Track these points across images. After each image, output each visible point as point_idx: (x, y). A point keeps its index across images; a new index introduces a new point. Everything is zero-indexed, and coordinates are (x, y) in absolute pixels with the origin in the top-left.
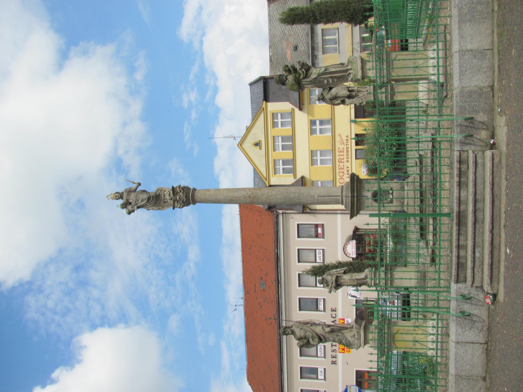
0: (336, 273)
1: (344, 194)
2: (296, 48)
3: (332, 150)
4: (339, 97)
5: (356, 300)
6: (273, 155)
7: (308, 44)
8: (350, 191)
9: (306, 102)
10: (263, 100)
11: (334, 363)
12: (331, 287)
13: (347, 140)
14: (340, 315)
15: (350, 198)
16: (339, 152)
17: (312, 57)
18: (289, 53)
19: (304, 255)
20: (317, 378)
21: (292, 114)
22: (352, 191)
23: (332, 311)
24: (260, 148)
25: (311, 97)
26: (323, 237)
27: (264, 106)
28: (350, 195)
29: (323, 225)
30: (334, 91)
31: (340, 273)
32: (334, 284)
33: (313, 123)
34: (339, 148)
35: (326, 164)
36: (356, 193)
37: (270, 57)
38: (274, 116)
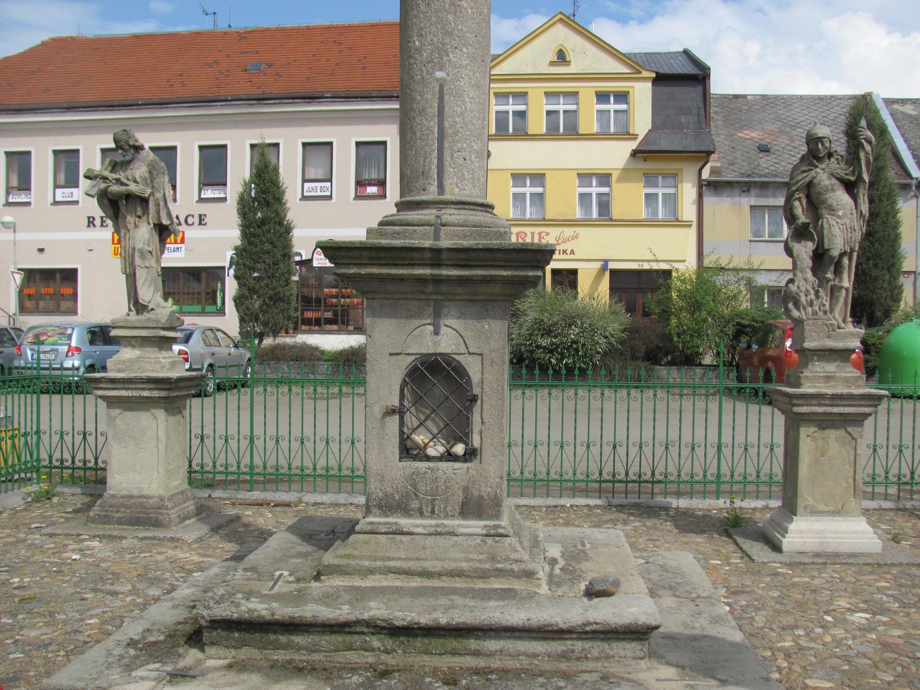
0: (159, 195)
1: (451, 215)
2: (764, 149)
3: (544, 219)
4: (817, 217)
5: (224, 268)
6: (536, 91)
7: (776, 176)
8: (466, 243)
9: (651, 166)
10: (657, 73)
11: (89, 222)
12: (105, 179)
13: (565, 252)
14: (191, 233)
15: (427, 244)
16: (540, 234)
17: (746, 182)
18: (753, 135)
19: (319, 156)
20: (56, 186)
21: (626, 135)
22: (464, 256)
23: (200, 216)
24: (552, 63)
25: (660, 178)
26: (357, 197)
27: (645, 74)
28: (445, 243)
29: (385, 197)
30: (841, 197)
31: (158, 212)
32: (115, 188)
33: (605, 179)
34: (548, 234)
35: (514, 206)
36: (454, 272)
37: (744, 97)
38: (622, 97)
